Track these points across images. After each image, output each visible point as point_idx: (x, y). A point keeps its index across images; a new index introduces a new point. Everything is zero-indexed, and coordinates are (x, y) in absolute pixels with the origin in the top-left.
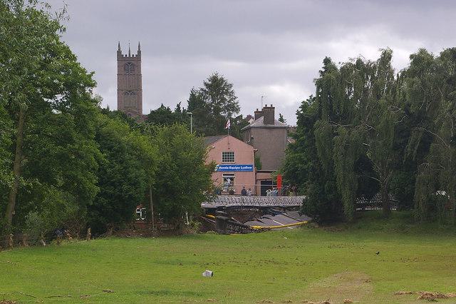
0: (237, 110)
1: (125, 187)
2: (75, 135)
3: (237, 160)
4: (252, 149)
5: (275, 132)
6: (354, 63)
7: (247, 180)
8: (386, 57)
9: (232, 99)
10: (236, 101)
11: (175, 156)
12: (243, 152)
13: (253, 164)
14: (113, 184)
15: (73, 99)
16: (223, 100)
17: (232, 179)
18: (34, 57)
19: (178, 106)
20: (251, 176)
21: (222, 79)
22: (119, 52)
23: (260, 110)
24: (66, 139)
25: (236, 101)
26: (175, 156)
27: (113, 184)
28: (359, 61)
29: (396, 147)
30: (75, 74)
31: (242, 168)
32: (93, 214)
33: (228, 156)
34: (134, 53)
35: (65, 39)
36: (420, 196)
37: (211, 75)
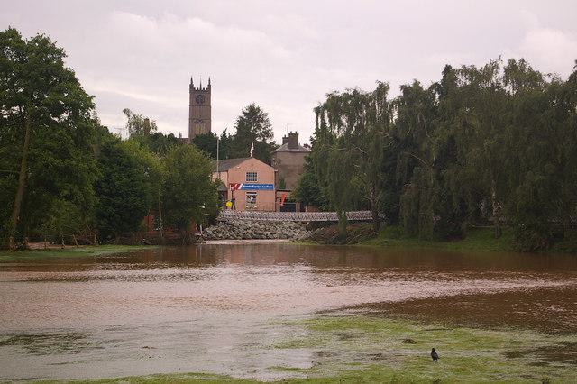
0: (271, 136)
1: (131, 198)
2: (72, 151)
3: (259, 180)
4: (272, 170)
5: (299, 155)
6: (351, 93)
7: (267, 198)
8: (382, 89)
9: (244, 120)
10: (270, 128)
11: (182, 171)
12: (265, 173)
13: (273, 183)
14: (121, 195)
15: (75, 116)
16: (259, 127)
17: (254, 197)
18: (26, 75)
19: (224, 132)
20: (271, 195)
21: (258, 109)
22: (192, 86)
23: (287, 136)
24: (63, 154)
25: (270, 128)
26: (182, 171)
27: (121, 195)
28: (355, 92)
29: (385, 170)
30: (77, 95)
31: (263, 187)
32: (102, 222)
33: (252, 176)
34: (205, 86)
35: (68, 63)
36: (405, 214)
37: (249, 104)
